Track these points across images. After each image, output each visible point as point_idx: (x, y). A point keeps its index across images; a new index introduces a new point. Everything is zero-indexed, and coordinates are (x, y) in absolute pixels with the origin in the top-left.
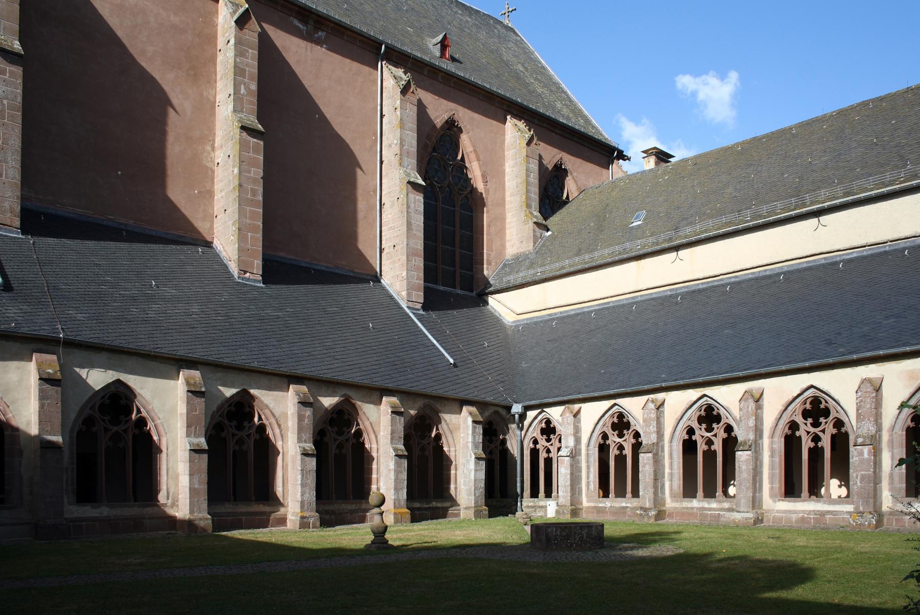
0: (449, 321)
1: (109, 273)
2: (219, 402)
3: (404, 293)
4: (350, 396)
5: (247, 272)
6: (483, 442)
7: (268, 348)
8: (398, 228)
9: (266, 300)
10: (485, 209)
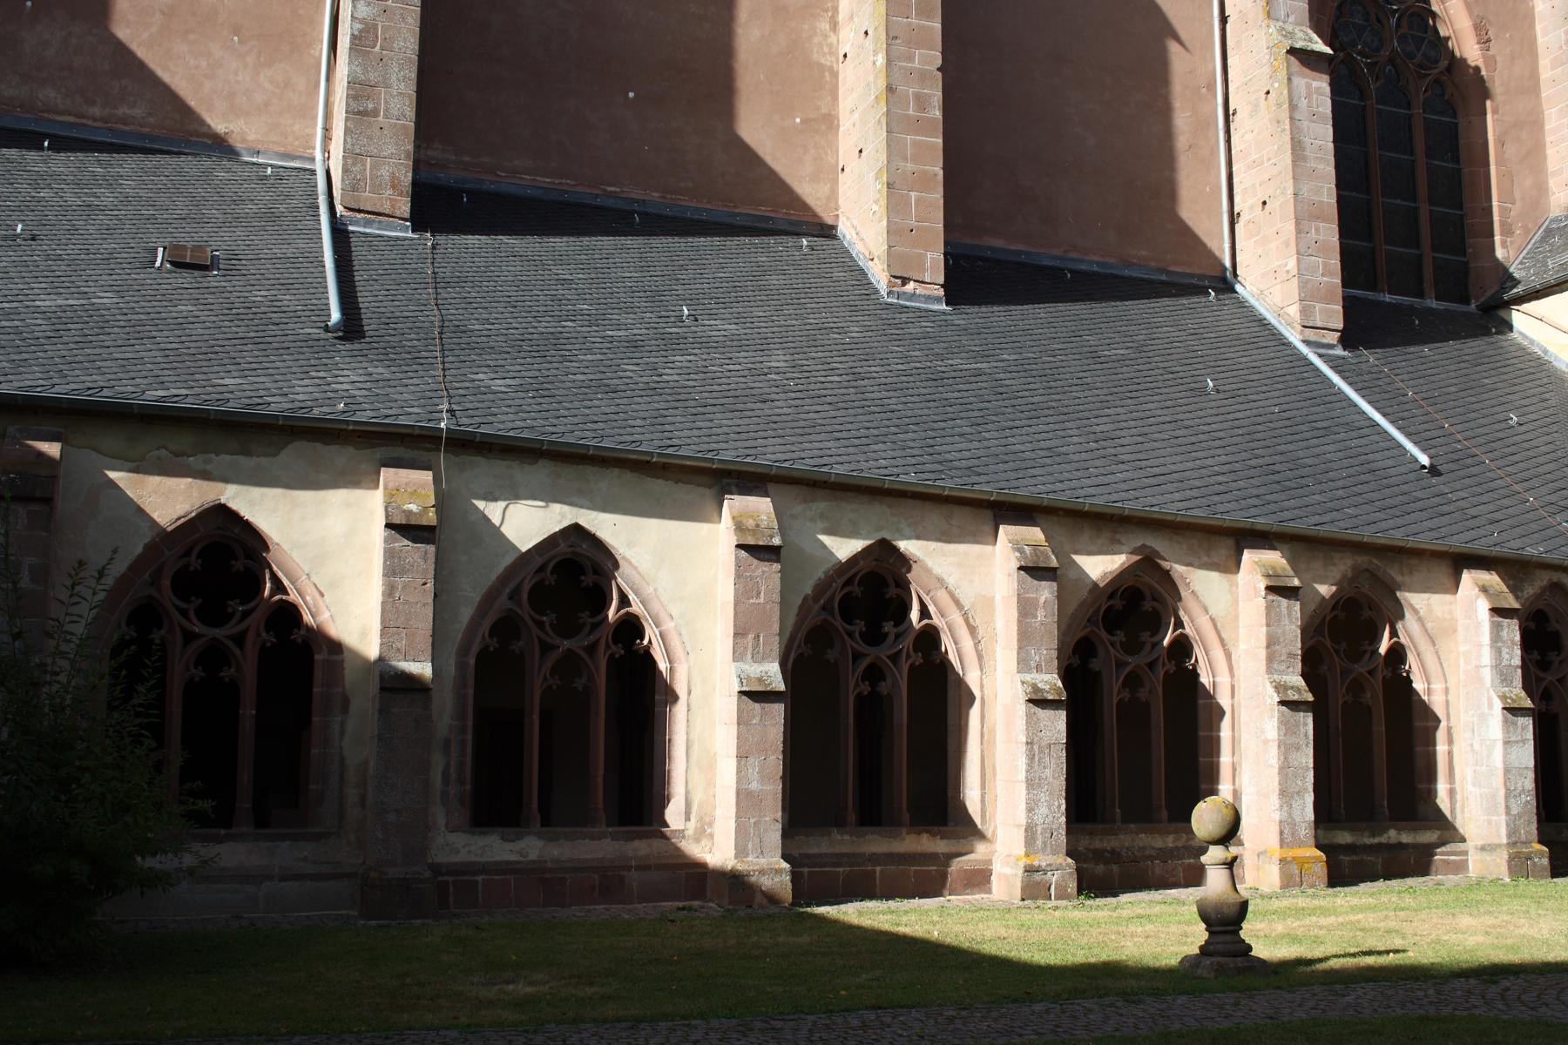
0: (1410, 369)
1: (588, 296)
2: (820, 573)
3: (1294, 311)
4: (1157, 552)
5: (911, 280)
6: (1524, 667)
7: (948, 440)
8: (1269, 159)
9: (950, 339)
10: (1488, 103)
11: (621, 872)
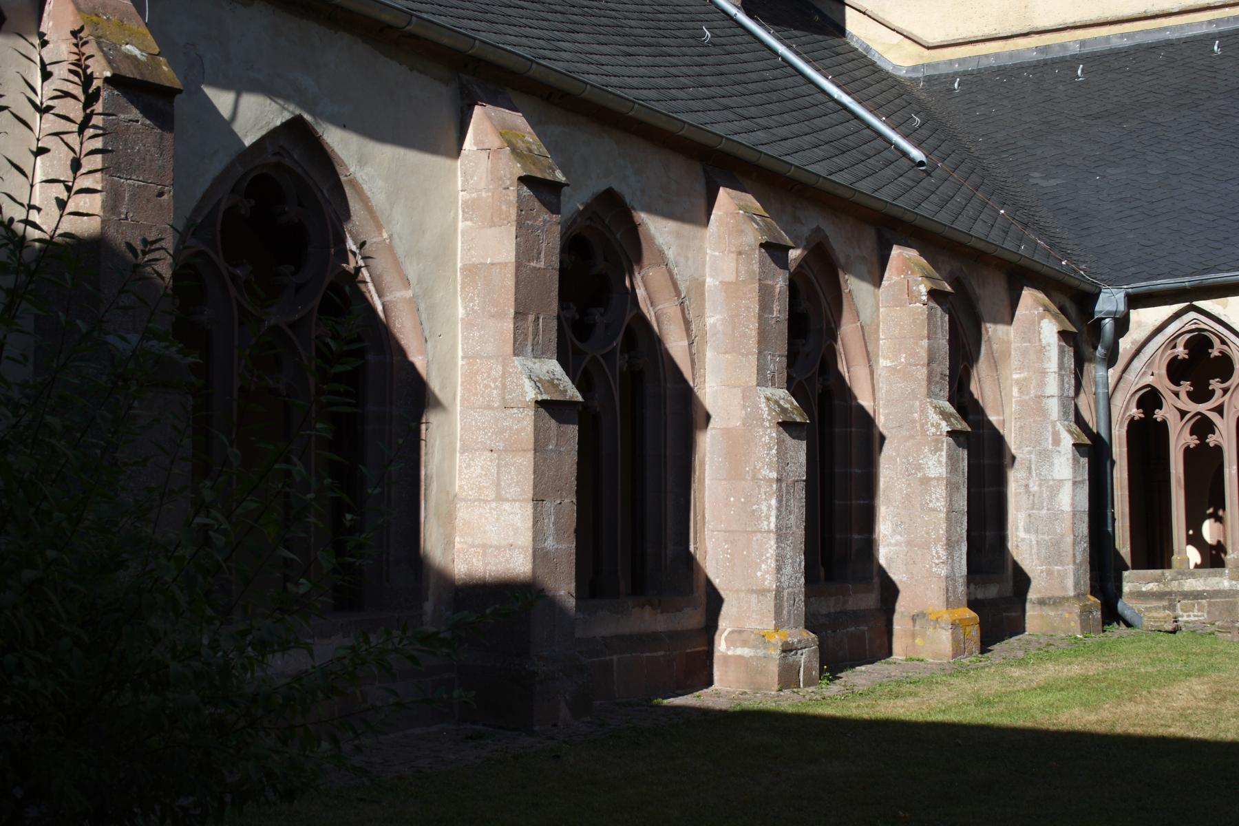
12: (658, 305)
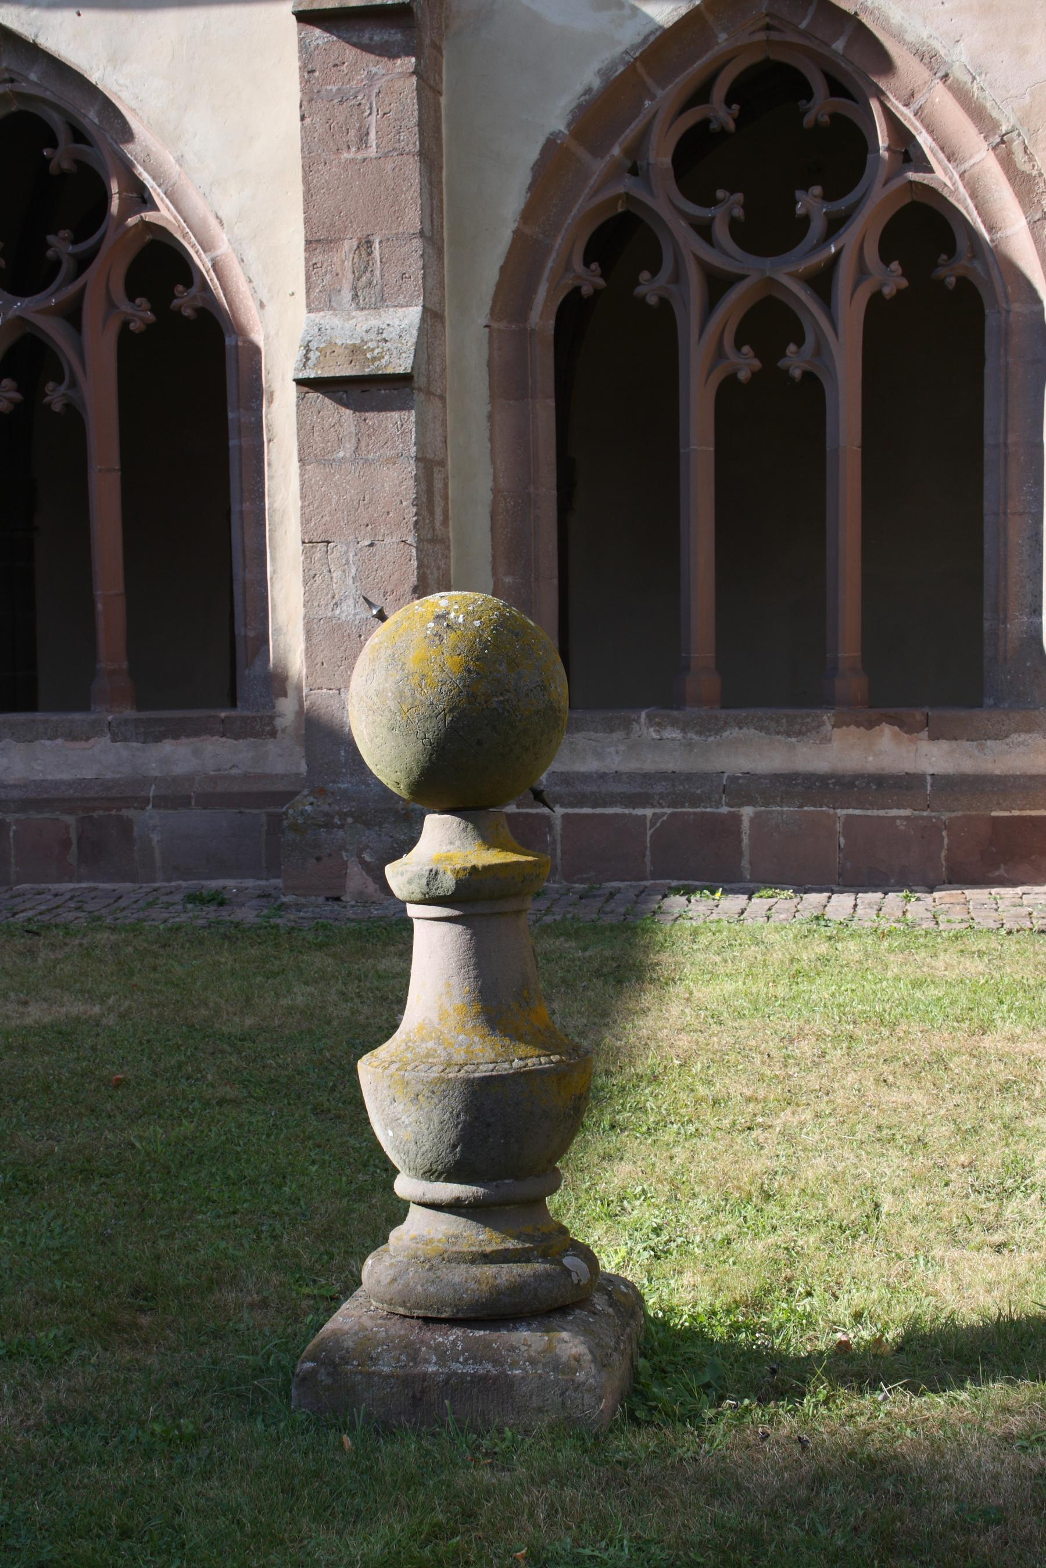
11: (125, 812)
12: (971, 157)
